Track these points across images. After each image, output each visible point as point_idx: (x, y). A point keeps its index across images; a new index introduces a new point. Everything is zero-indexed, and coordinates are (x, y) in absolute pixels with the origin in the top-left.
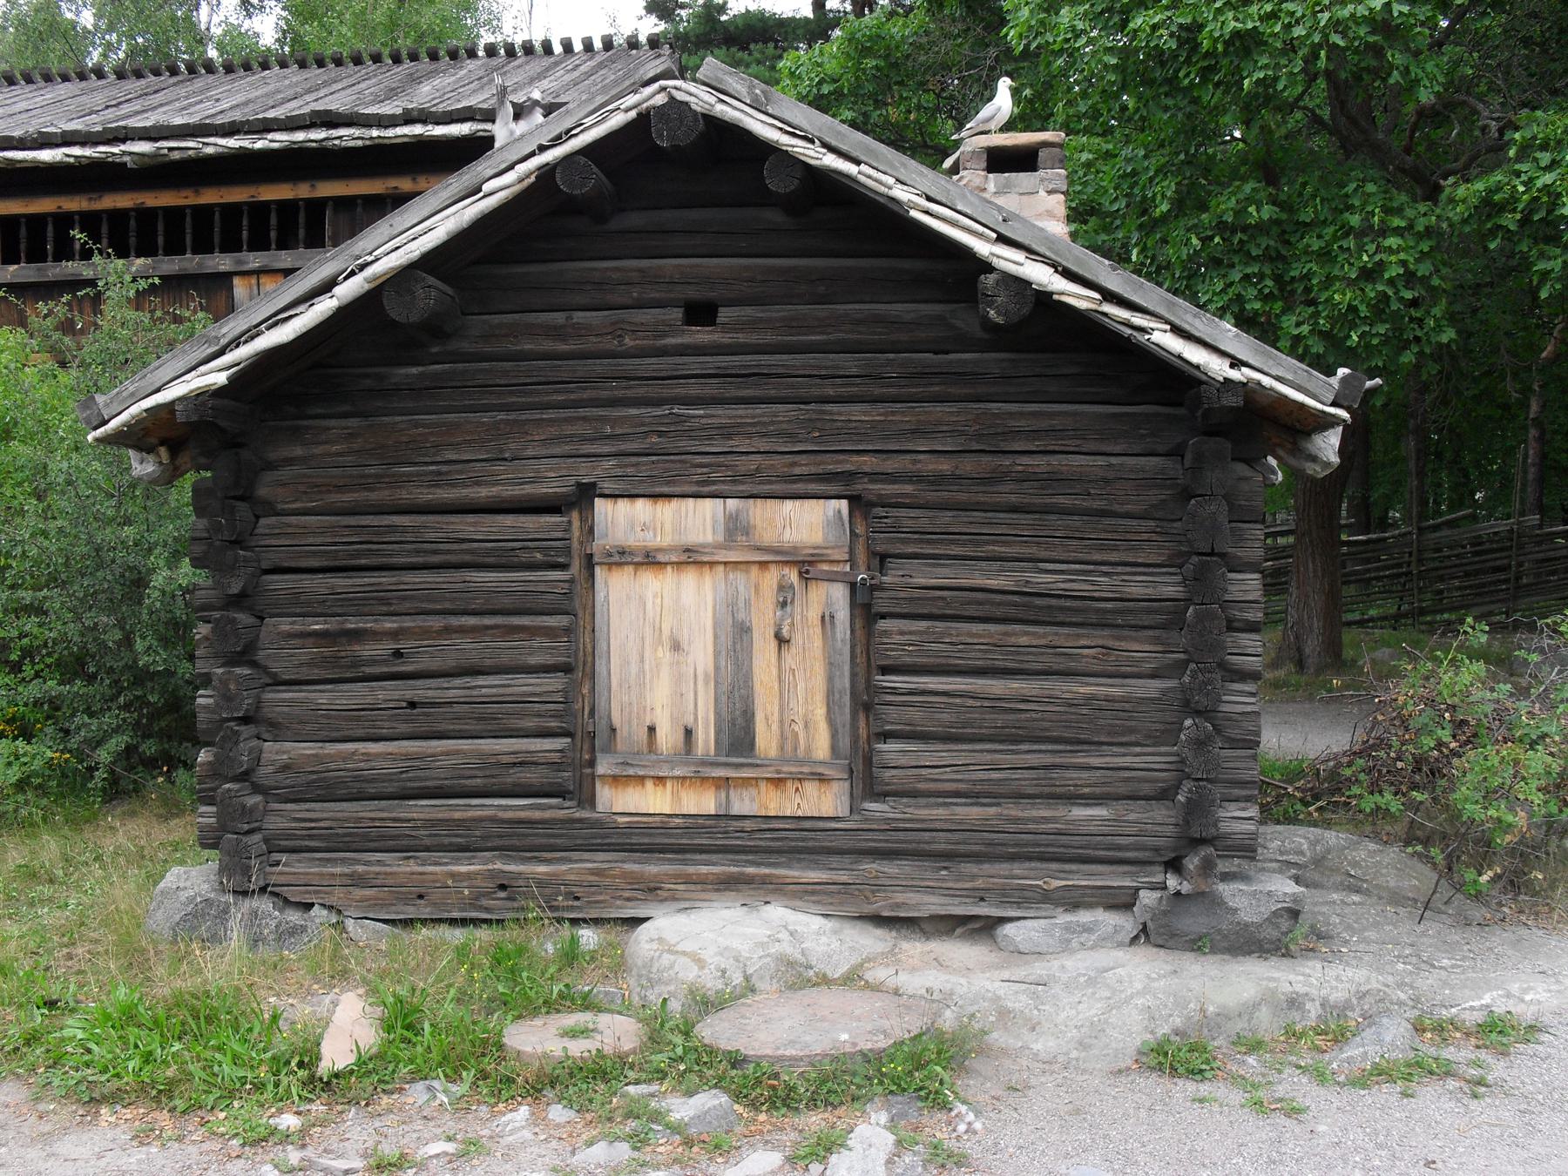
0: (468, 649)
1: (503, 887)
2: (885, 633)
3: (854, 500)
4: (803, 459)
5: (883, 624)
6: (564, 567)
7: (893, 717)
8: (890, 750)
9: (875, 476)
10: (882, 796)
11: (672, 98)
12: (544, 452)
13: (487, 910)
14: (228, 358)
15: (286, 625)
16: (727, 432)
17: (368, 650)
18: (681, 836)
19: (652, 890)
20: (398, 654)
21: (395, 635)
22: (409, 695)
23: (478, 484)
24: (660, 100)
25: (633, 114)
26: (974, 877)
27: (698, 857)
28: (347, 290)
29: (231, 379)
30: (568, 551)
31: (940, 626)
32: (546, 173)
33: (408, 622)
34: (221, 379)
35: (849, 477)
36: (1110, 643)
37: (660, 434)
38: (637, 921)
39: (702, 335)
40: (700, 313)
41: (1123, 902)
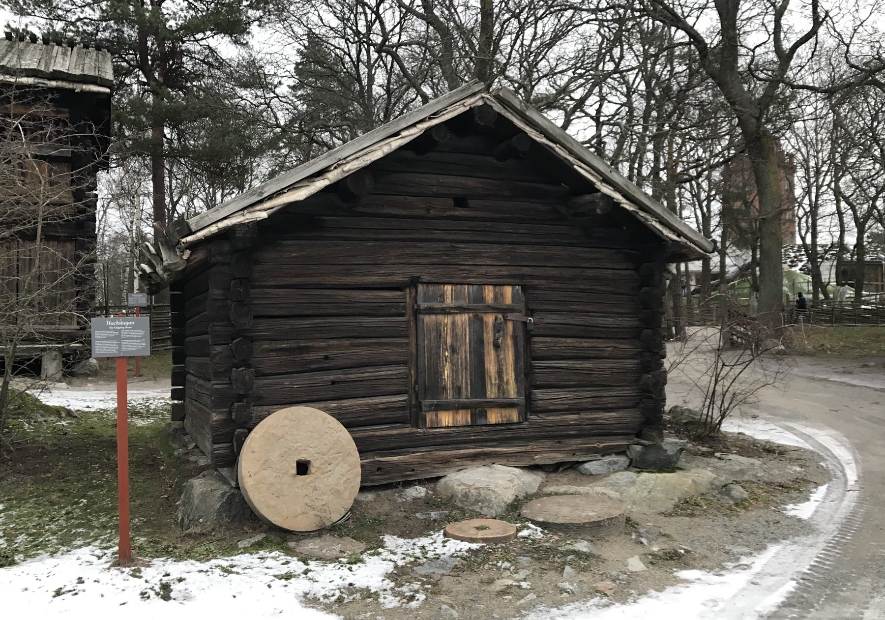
0: (364, 353)
1: (379, 469)
2: (536, 342)
3: (524, 288)
4: (504, 268)
5: (535, 339)
6: (402, 315)
7: (540, 379)
8: (539, 394)
9: (532, 277)
10: (536, 412)
11: (485, 103)
12: (397, 261)
13: (372, 481)
14: (267, 205)
15: (266, 346)
16: (474, 255)
17: (312, 356)
18: (456, 436)
19: (446, 462)
20: (326, 358)
21: (324, 349)
22: (332, 377)
23: (366, 275)
24: (480, 103)
25: (468, 108)
26: (571, 446)
27: (462, 446)
28: (333, 176)
29: (270, 216)
30: (404, 307)
31: (556, 339)
32: (429, 130)
33: (332, 342)
34: (264, 215)
35: (522, 276)
36: (617, 345)
37: (447, 255)
38: (439, 478)
39: (460, 212)
40: (460, 202)
41: (621, 452)
